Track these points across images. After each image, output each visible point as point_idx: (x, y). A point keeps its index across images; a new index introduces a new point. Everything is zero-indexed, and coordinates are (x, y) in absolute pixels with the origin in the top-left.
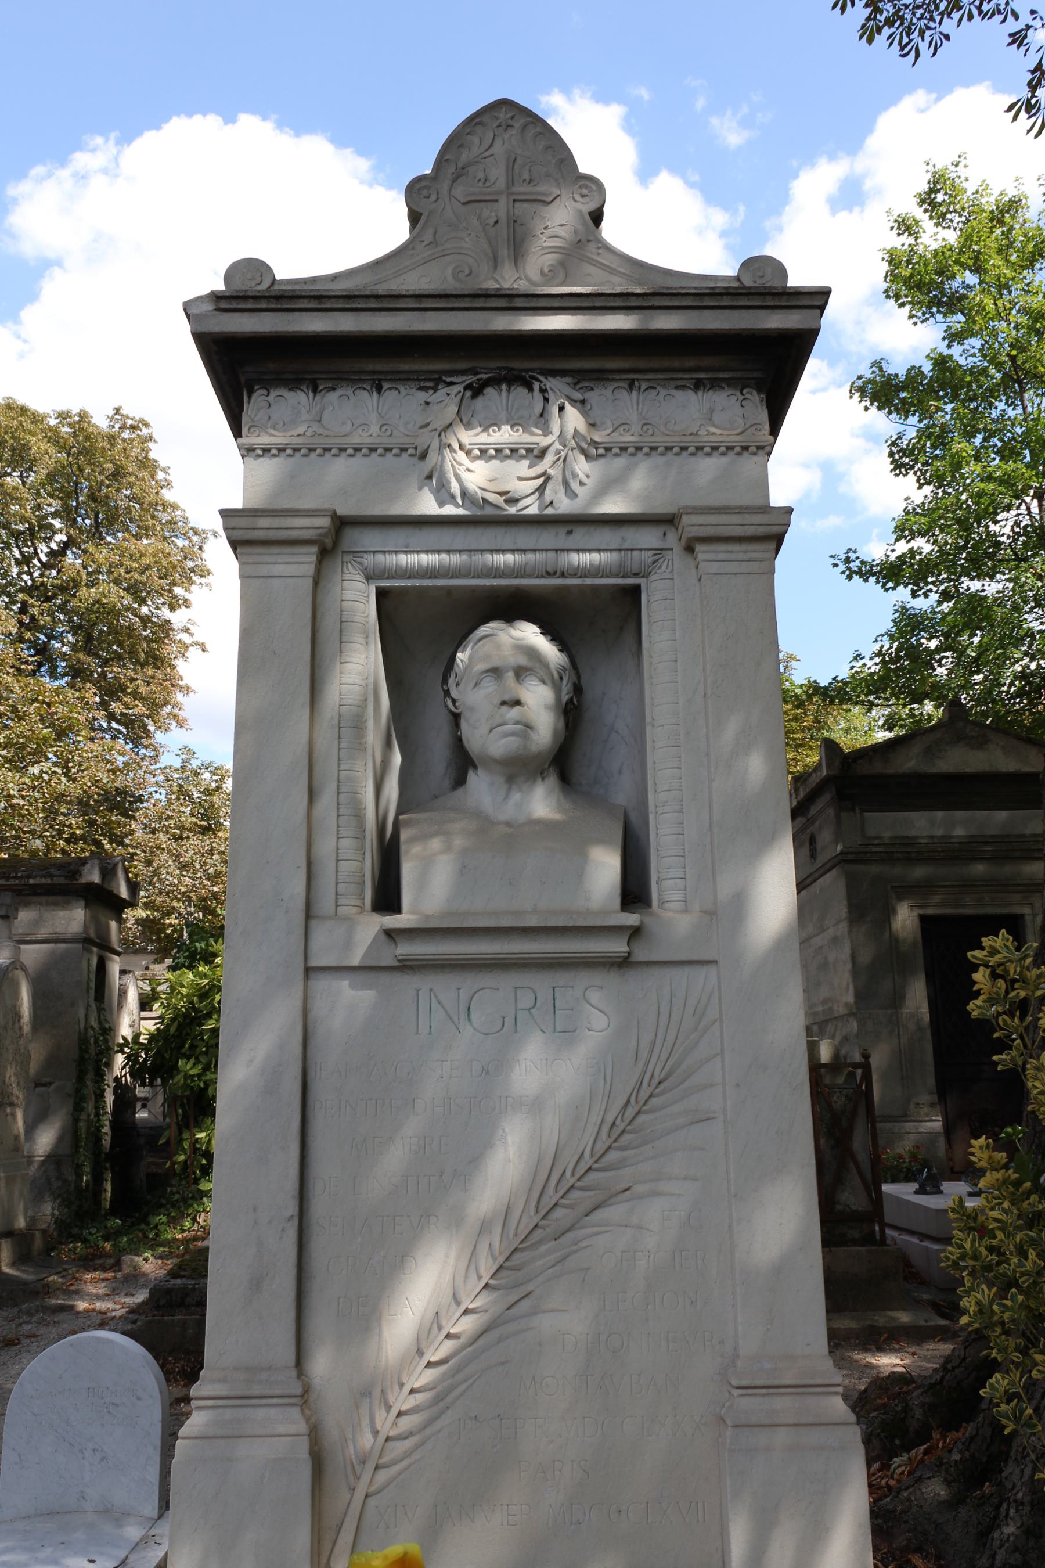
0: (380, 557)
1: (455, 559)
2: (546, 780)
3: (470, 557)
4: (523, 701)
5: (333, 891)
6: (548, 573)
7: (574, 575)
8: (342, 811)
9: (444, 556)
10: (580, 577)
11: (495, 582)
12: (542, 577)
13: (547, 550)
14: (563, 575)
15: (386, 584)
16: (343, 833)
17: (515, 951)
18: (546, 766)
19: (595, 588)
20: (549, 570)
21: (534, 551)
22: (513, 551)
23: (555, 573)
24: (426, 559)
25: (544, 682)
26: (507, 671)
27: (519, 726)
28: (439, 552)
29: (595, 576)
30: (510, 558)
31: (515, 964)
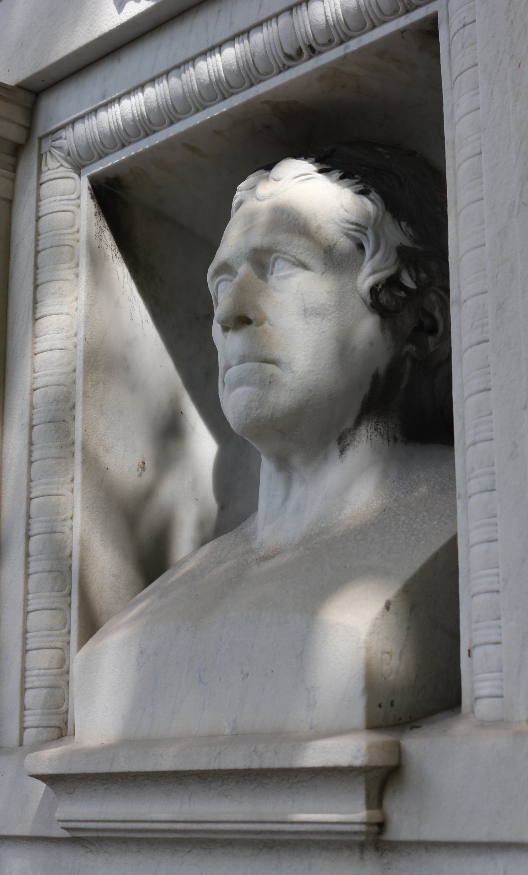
0: (80, 127)
1: (153, 94)
2: (350, 453)
3: (180, 77)
4: (251, 316)
5: (17, 703)
6: (289, 57)
7: (330, 44)
8: (34, 567)
9: (149, 91)
10: (342, 42)
11: (223, 107)
12: (285, 68)
13: (277, 16)
14: (313, 52)
15: (98, 168)
16: (33, 605)
17: (148, 817)
18: (350, 423)
19: (380, 49)
20: (289, 51)
21: (259, 25)
22: (231, 40)
23: (300, 52)
24: (132, 106)
25: (305, 267)
26: (239, 265)
27: (248, 365)
28: (141, 87)
29: (362, 30)
30: (230, 55)
31: (139, 842)
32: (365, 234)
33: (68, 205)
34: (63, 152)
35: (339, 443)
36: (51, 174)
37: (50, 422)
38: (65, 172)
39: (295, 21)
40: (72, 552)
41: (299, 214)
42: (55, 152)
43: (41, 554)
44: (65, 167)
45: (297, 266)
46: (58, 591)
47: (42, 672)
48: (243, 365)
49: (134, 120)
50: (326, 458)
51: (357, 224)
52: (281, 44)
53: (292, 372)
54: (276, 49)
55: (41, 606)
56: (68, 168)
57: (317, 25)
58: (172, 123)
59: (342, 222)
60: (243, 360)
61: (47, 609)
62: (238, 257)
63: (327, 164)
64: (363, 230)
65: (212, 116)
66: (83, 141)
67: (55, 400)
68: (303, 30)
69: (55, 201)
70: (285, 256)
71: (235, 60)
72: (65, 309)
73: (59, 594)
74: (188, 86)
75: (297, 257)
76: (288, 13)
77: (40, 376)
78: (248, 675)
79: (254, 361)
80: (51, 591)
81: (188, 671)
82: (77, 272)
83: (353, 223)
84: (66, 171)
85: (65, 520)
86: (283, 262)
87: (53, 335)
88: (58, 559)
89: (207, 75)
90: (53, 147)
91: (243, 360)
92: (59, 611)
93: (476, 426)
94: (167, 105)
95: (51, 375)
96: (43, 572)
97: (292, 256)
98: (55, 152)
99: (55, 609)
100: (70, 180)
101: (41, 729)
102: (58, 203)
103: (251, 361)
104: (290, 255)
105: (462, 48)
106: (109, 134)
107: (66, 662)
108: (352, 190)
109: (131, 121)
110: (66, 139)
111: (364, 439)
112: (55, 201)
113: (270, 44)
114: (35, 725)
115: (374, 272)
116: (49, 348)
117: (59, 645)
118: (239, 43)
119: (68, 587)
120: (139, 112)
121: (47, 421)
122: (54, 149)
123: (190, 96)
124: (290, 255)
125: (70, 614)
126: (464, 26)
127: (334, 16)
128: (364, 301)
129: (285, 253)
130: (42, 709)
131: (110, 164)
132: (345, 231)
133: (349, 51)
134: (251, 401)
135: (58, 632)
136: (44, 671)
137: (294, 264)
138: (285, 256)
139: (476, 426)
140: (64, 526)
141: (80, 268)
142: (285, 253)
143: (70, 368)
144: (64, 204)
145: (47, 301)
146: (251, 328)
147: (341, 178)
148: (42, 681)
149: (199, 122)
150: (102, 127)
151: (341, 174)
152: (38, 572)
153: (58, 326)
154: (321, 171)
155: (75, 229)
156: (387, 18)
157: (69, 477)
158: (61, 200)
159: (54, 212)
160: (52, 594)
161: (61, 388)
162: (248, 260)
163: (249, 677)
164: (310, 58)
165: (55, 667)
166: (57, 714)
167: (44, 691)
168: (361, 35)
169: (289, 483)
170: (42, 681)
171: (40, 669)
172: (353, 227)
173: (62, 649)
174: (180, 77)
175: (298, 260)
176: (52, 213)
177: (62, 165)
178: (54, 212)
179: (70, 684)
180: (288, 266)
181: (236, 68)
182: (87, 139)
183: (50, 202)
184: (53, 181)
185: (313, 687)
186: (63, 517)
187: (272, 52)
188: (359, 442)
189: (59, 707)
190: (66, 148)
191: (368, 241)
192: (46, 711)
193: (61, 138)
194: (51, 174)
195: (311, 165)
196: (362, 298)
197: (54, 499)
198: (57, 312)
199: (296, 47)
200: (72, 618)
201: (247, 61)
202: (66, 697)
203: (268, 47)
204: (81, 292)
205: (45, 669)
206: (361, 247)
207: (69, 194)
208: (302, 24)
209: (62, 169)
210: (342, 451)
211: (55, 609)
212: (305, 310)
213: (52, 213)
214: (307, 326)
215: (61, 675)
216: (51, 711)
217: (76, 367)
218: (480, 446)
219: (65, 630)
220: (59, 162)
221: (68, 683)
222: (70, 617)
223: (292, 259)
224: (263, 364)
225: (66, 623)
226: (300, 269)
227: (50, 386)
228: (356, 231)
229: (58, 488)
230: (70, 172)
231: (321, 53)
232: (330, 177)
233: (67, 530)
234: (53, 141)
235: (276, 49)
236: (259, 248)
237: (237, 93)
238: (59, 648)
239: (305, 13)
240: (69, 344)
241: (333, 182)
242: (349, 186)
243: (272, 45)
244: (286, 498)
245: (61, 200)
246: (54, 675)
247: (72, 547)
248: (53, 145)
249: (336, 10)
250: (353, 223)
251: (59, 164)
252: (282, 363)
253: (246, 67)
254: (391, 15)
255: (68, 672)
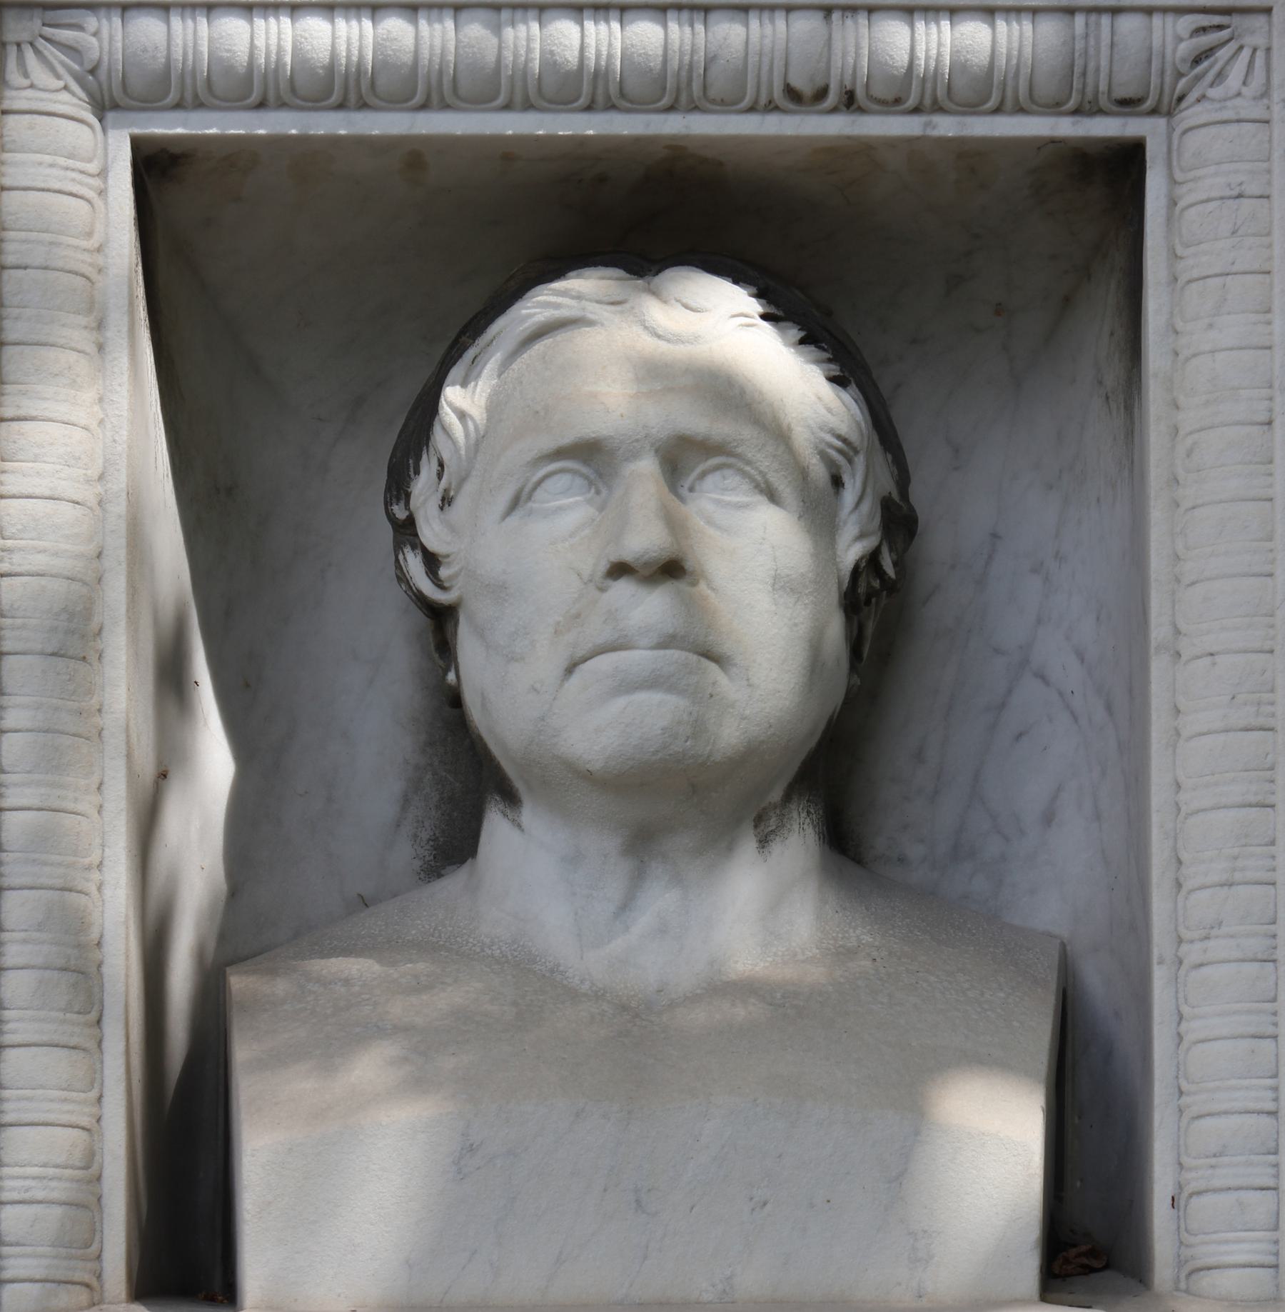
2: (776, 847)
7: (893, 104)
12: (772, 107)
14: (849, 102)
18: (776, 795)
20: (798, 82)
23: (822, 94)
25: (772, 496)
26: (634, 455)
27: (675, 654)
29: (972, 108)
32: (850, 461)
33: (81, 183)
34: (81, 64)
35: (756, 827)
36: (42, 100)
37: (53, 654)
38: (74, 105)
39: (837, 36)
40: (102, 936)
41: (761, 393)
42: (50, 51)
43: (39, 931)
44: (73, 94)
45: (761, 491)
46: (79, 1013)
47: (51, 1171)
48: (668, 652)
49: (331, 68)
50: (730, 848)
51: (844, 440)
52: (787, 65)
53: (750, 685)
54: (771, 70)
55: (45, 1038)
56: (80, 99)
57: (886, 64)
58: (424, 106)
59: (821, 429)
60: (667, 642)
61: (57, 1046)
62: (637, 441)
63: (785, 306)
64: (851, 453)
65: (551, 132)
66: (154, 57)
67: (65, 610)
68: (851, 60)
69: (52, 166)
70: (748, 468)
71: (660, 52)
72: (80, 416)
73: (81, 1018)
74: (516, 56)
75: (768, 476)
76: (820, 15)
77: (20, 549)
78: (765, 1204)
79: (689, 651)
80: (65, 1010)
81: (605, 1190)
82: (101, 340)
83: (839, 437)
84: (74, 102)
85: (88, 868)
86: (738, 478)
87: (58, 467)
88: (79, 946)
89: (576, 53)
90: (41, 36)
91: (667, 642)
92: (82, 1054)
93: (1236, 858)
94: (441, 72)
95: (56, 554)
96: (46, 968)
97: (761, 472)
98: (52, 53)
99: (74, 1048)
100: (85, 128)
101: (53, 1285)
102: (62, 173)
103: (682, 649)
104: (757, 469)
105: (1233, 233)
106: (242, 70)
107: (97, 1158)
108: (824, 371)
109: (323, 67)
110: (95, 34)
111: (796, 827)
112: (52, 166)
113: (761, 55)
114: (38, 1277)
115: (861, 536)
116: (47, 493)
117: (85, 1121)
118: (680, 25)
119: (96, 1008)
120: (355, 59)
121: (50, 650)
122: (48, 45)
123: (512, 77)
124: (757, 469)
125: (102, 1062)
126: (1240, 196)
127: (932, 64)
128: (840, 583)
129: (749, 463)
130: (53, 1245)
131: (213, 131)
132: (822, 446)
133: (936, 133)
134: (679, 723)
135: (83, 1095)
136: (57, 1170)
137: (757, 486)
138: (748, 468)
139: (1236, 858)
140: (87, 880)
141: (109, 334)
142: (749, 463)
143: (91, 549)
144: (73, 180)
145: (39, 388)
146: (681, 585)
147: (802, 342)
148: (53, 1189)
149: (510, 132)
150: (229, 51)
151: (802, 334)
152: (33, 967)
153: (69, 449)
154: (765, 317)
155: (93, 243)
156: (1035, 107)
157: (95, 780)
158: (67, 169)
159: (48, 190)
160: (68, 1015)
161: (76, 586)
162: (657, 451)
163: (769, 1207)
164: (834, 110)
165: (78, 1164)
166: (84, 1259)
167: (58, 1211)
168: (964, 114)
169: (638, 879)
170: (53, 1189)
171: (44, 1166)
172: (839, 444)
173: (88, 1130)
174: (497, 30)
175: (767, 482)
176: (43, 190)
177: (66, 88)
178: (48, 190)
179: (104, 1201)
180: (746, 486)
181: (659, 67)
182: (168, 57)
183: (40, 164)
184: (45, 118)
185: (925, 1232)
186: (87, 861)
187: (759, 69)
188: (790, 830)
189: (87, 1246)
190: (95, 55)
191: (853, 475)
192: (63, 1251)
193: (80, 28)
194: (42, 100)
195: (753, 300)
196: (839, 578)
197: (68, 820)
198: (65, 418)
199: (820, 82)
200: (106, 1072)
201: (691, 65)
202: (98, 1228)
203: (753, 59)
204: (119, 389)
205: (57, 1166)
206: (837, 482)
207: (82, 160)
208: (852, 49)
209: (65, 96)
210: (764, 842)
211: (74, 1048)
212: (776, 578)
213: (43, 190)
214: (774, 608)
215: (89, 1182)
216: (73, 1251)
217: (102, 548)
218: (1242, 890)
219: (93, 1094)
220: (58, 77)
221: (99, 1199)
222: (102, 1068)
223: (759, 478)
224: (703, 660)
225: (95, 1079)
226: (762, 499)
227: (52, 576)
228: (840, 451)
229: (76, 800)
230: (85, 110)
231: (862, 110)
232: (782, 331)
233: (93, 889)
234: (44, 25)
235: (771, 70)
236: (700, 438)
237: (628, 111)
238: (83, 1128)
239: (864, 31)
240: (88, 494)
241: (787, 344)
242: (817, 362)
243: (766, 60)
244: (626, 906)
245: (67, 169)
246: (78, 1181)
247: (102, 925)
248: (43, 33)
249: (939, 54)
250: (839, 437)
251: (61, 84)
252: (735, 665)
253: (684, 73)
254: (1047, 106)
255: (99, 1178)
